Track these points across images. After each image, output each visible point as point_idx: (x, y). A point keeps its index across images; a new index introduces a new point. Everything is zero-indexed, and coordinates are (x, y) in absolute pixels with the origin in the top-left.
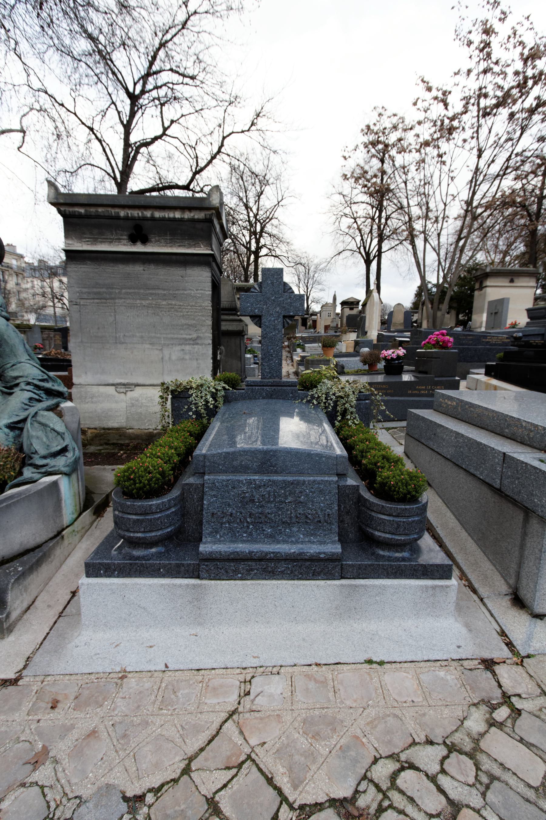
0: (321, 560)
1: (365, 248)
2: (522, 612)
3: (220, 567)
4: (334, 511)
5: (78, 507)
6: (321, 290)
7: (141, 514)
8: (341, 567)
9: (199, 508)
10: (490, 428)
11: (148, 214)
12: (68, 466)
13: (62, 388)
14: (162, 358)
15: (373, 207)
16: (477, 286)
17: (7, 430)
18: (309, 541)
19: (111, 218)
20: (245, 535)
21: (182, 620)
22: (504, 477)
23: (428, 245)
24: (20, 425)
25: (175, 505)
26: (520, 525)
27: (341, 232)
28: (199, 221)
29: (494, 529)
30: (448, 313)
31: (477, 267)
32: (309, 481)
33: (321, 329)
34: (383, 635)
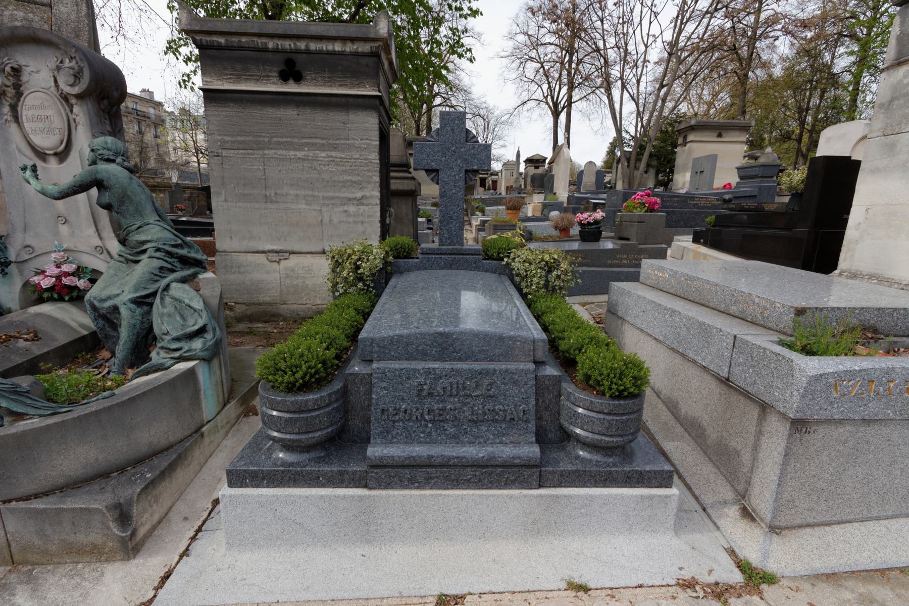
0: (516, 466)
1: (552, 98)
2: (752, 524)
3: (392, 474)
4: (531, 406)
5: (221, 398)
6: (502, 146)
7: (294, 412)
8: (540, 475)
9: (366, 403)
10: (711, 304)
11: (302, 45)
12: (207, 349)
13: (200, 256)
14: (321, 221)
15: (562, 49)
16: (680, 141)
17: (132, 306)
18: (500, 443)
19: (257, 50)
20: (422, 435)
21: (347, 537)
22: (733, 365)
23: (626, 94)
24: (149, 300)
25: (337, 400)
26: (755, 422)
27: (526, 79)
28: (363, 55)
29: (719, 425)
30: (646, 172)
31: (680, 119)
32: (500, 370)
33: (502, 189)
34: (589, 555)
